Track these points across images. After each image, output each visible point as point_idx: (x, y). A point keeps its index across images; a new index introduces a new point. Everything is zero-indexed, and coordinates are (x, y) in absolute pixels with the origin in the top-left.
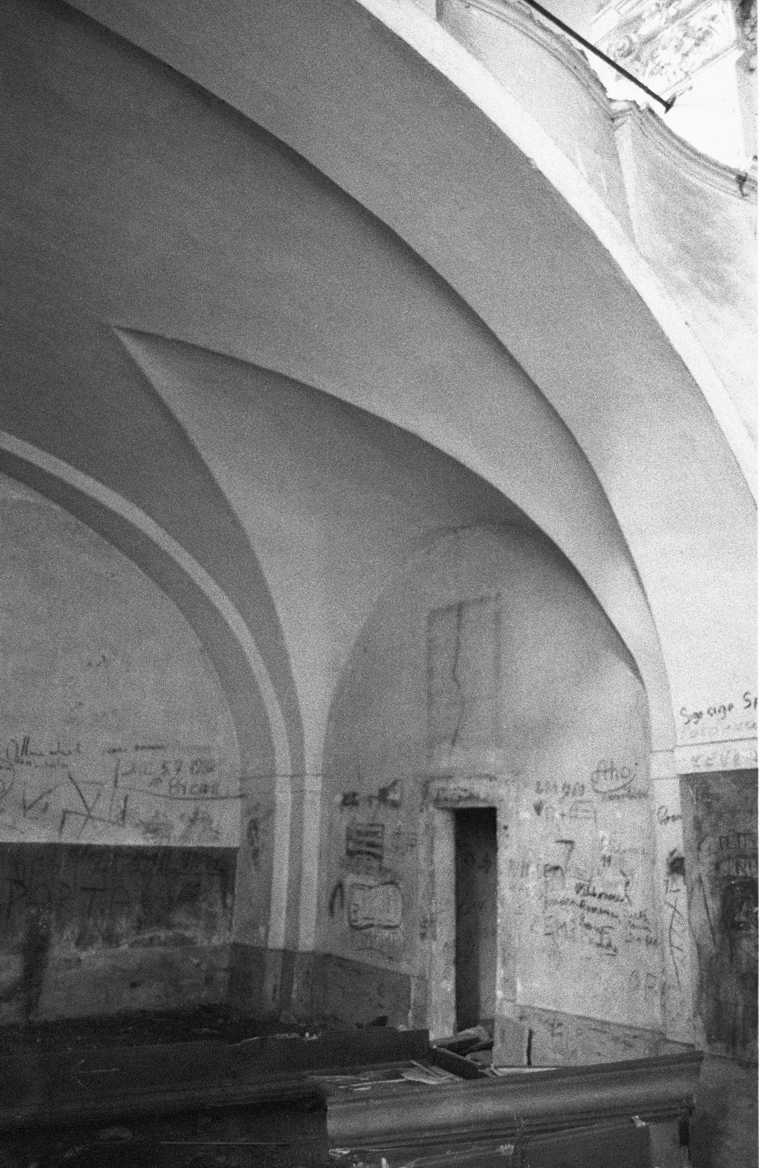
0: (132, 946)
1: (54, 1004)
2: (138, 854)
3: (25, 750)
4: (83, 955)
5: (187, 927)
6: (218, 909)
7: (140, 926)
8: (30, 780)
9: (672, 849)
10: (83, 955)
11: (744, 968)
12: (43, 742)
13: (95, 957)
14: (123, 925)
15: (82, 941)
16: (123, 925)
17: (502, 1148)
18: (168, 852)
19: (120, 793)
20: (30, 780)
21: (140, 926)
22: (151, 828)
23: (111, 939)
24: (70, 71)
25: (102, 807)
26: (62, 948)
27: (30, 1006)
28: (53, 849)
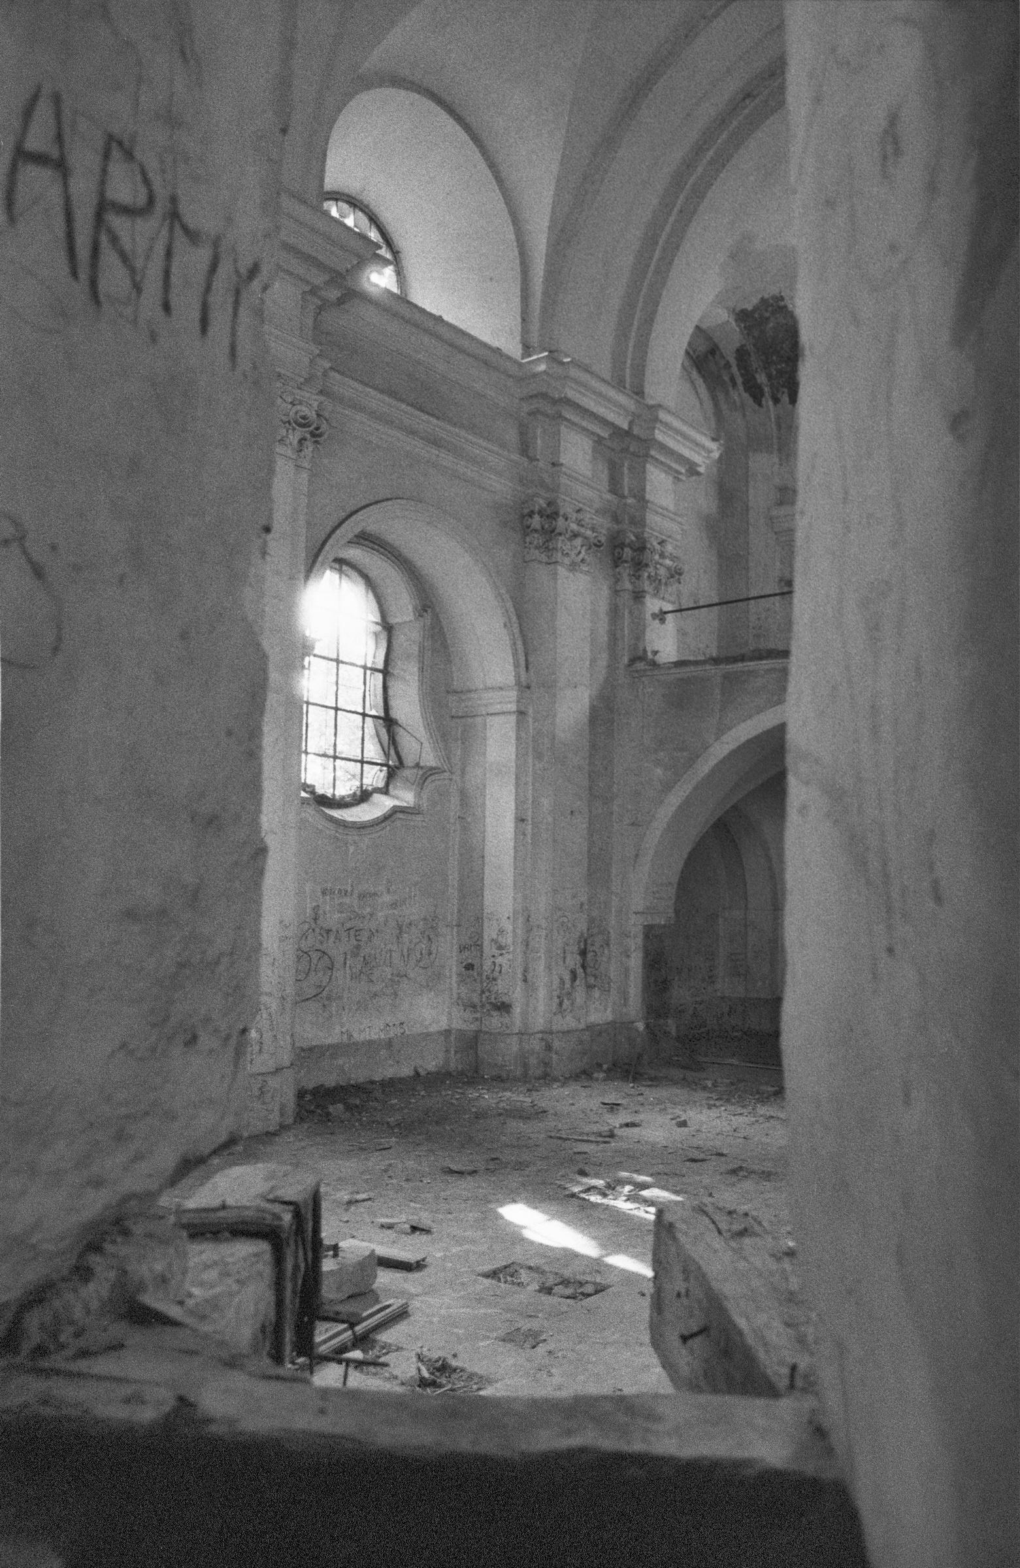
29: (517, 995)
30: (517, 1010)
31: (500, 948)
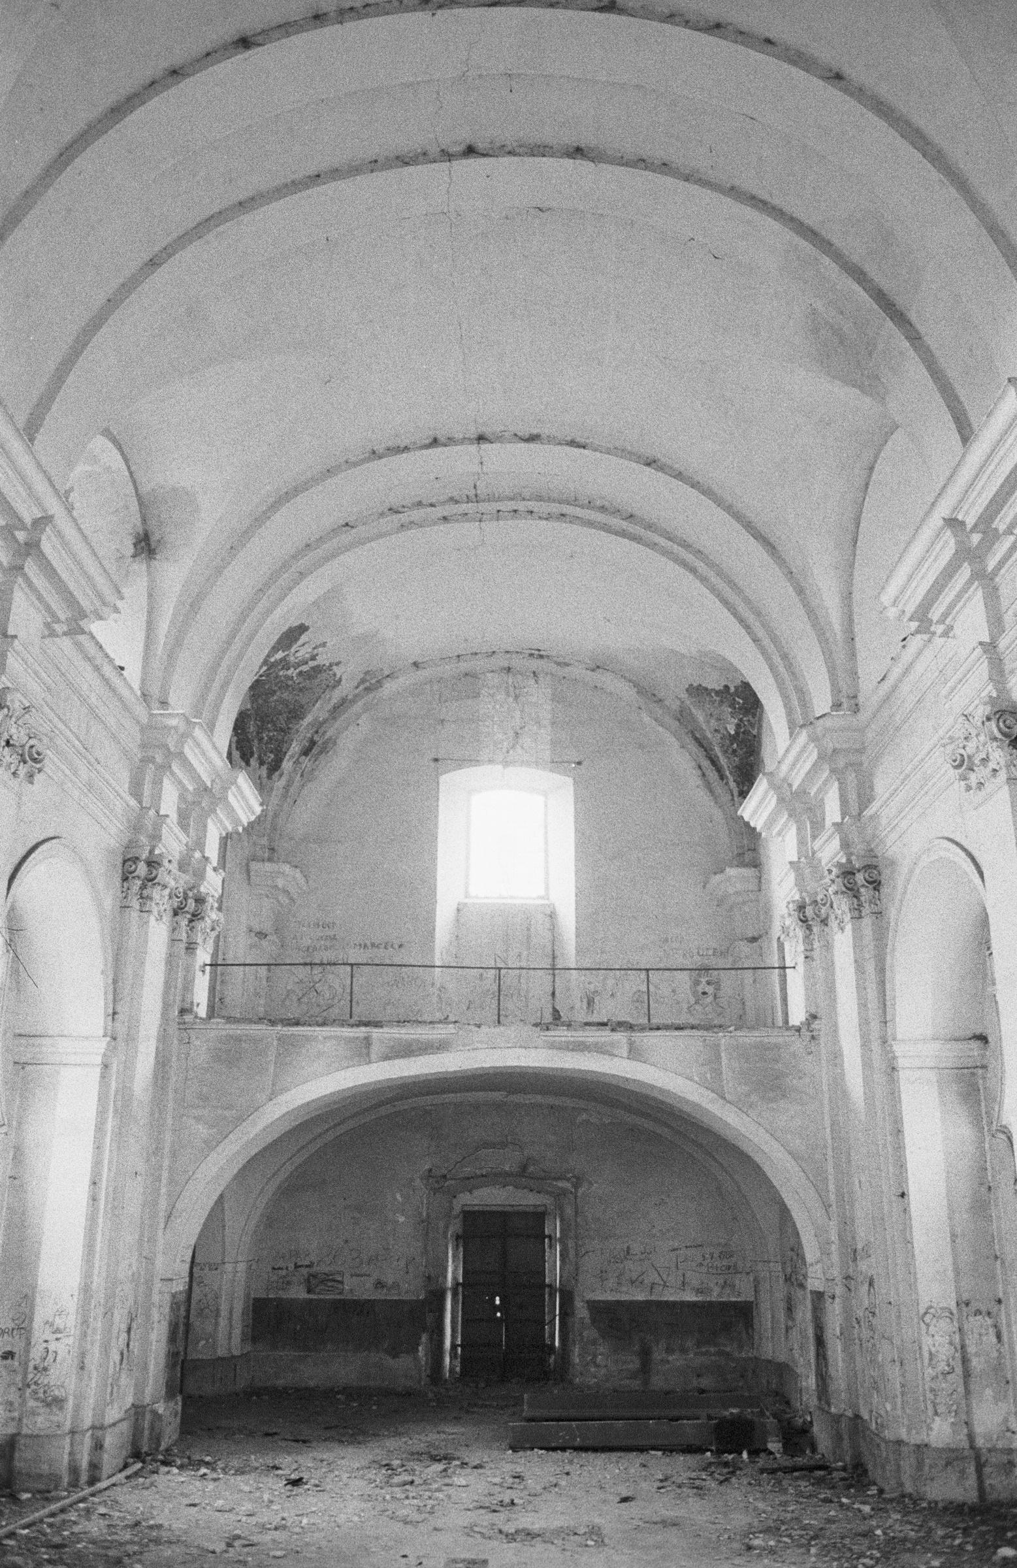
0: (696, 1354)
1: (657, 1382)
2: (694, 1305)
3: (628, 1253)
4: (670, 1358)
5: (725, 1346)
6: (744, 1335)
7: (699, 1344)
8: (632, 1268)
9: (990, 1039)
10: (670, 1358)
11: (675, 706)
12: (636, 1248)
13: (676, 1359)
14: (689, 1344)
15: (669, 1350)
16: (689, 1344)
17: (498, 1298)
18: (710, 1303)
19: (680, 1272)
20: (632, 1268)
21: (699, 1344)
22: (699, 1291)
23: (684, 1351)
24: (409, 925)
25: (671, 1280)
26: (658, 1355)
27: (646, 1382)
28: (648, 1303)
29: (71, 1384)
30: (70, 1404)
31: (58, 1331)
